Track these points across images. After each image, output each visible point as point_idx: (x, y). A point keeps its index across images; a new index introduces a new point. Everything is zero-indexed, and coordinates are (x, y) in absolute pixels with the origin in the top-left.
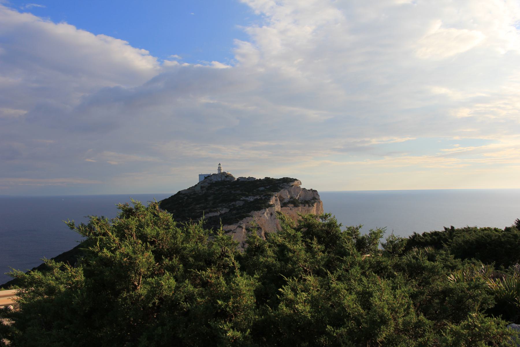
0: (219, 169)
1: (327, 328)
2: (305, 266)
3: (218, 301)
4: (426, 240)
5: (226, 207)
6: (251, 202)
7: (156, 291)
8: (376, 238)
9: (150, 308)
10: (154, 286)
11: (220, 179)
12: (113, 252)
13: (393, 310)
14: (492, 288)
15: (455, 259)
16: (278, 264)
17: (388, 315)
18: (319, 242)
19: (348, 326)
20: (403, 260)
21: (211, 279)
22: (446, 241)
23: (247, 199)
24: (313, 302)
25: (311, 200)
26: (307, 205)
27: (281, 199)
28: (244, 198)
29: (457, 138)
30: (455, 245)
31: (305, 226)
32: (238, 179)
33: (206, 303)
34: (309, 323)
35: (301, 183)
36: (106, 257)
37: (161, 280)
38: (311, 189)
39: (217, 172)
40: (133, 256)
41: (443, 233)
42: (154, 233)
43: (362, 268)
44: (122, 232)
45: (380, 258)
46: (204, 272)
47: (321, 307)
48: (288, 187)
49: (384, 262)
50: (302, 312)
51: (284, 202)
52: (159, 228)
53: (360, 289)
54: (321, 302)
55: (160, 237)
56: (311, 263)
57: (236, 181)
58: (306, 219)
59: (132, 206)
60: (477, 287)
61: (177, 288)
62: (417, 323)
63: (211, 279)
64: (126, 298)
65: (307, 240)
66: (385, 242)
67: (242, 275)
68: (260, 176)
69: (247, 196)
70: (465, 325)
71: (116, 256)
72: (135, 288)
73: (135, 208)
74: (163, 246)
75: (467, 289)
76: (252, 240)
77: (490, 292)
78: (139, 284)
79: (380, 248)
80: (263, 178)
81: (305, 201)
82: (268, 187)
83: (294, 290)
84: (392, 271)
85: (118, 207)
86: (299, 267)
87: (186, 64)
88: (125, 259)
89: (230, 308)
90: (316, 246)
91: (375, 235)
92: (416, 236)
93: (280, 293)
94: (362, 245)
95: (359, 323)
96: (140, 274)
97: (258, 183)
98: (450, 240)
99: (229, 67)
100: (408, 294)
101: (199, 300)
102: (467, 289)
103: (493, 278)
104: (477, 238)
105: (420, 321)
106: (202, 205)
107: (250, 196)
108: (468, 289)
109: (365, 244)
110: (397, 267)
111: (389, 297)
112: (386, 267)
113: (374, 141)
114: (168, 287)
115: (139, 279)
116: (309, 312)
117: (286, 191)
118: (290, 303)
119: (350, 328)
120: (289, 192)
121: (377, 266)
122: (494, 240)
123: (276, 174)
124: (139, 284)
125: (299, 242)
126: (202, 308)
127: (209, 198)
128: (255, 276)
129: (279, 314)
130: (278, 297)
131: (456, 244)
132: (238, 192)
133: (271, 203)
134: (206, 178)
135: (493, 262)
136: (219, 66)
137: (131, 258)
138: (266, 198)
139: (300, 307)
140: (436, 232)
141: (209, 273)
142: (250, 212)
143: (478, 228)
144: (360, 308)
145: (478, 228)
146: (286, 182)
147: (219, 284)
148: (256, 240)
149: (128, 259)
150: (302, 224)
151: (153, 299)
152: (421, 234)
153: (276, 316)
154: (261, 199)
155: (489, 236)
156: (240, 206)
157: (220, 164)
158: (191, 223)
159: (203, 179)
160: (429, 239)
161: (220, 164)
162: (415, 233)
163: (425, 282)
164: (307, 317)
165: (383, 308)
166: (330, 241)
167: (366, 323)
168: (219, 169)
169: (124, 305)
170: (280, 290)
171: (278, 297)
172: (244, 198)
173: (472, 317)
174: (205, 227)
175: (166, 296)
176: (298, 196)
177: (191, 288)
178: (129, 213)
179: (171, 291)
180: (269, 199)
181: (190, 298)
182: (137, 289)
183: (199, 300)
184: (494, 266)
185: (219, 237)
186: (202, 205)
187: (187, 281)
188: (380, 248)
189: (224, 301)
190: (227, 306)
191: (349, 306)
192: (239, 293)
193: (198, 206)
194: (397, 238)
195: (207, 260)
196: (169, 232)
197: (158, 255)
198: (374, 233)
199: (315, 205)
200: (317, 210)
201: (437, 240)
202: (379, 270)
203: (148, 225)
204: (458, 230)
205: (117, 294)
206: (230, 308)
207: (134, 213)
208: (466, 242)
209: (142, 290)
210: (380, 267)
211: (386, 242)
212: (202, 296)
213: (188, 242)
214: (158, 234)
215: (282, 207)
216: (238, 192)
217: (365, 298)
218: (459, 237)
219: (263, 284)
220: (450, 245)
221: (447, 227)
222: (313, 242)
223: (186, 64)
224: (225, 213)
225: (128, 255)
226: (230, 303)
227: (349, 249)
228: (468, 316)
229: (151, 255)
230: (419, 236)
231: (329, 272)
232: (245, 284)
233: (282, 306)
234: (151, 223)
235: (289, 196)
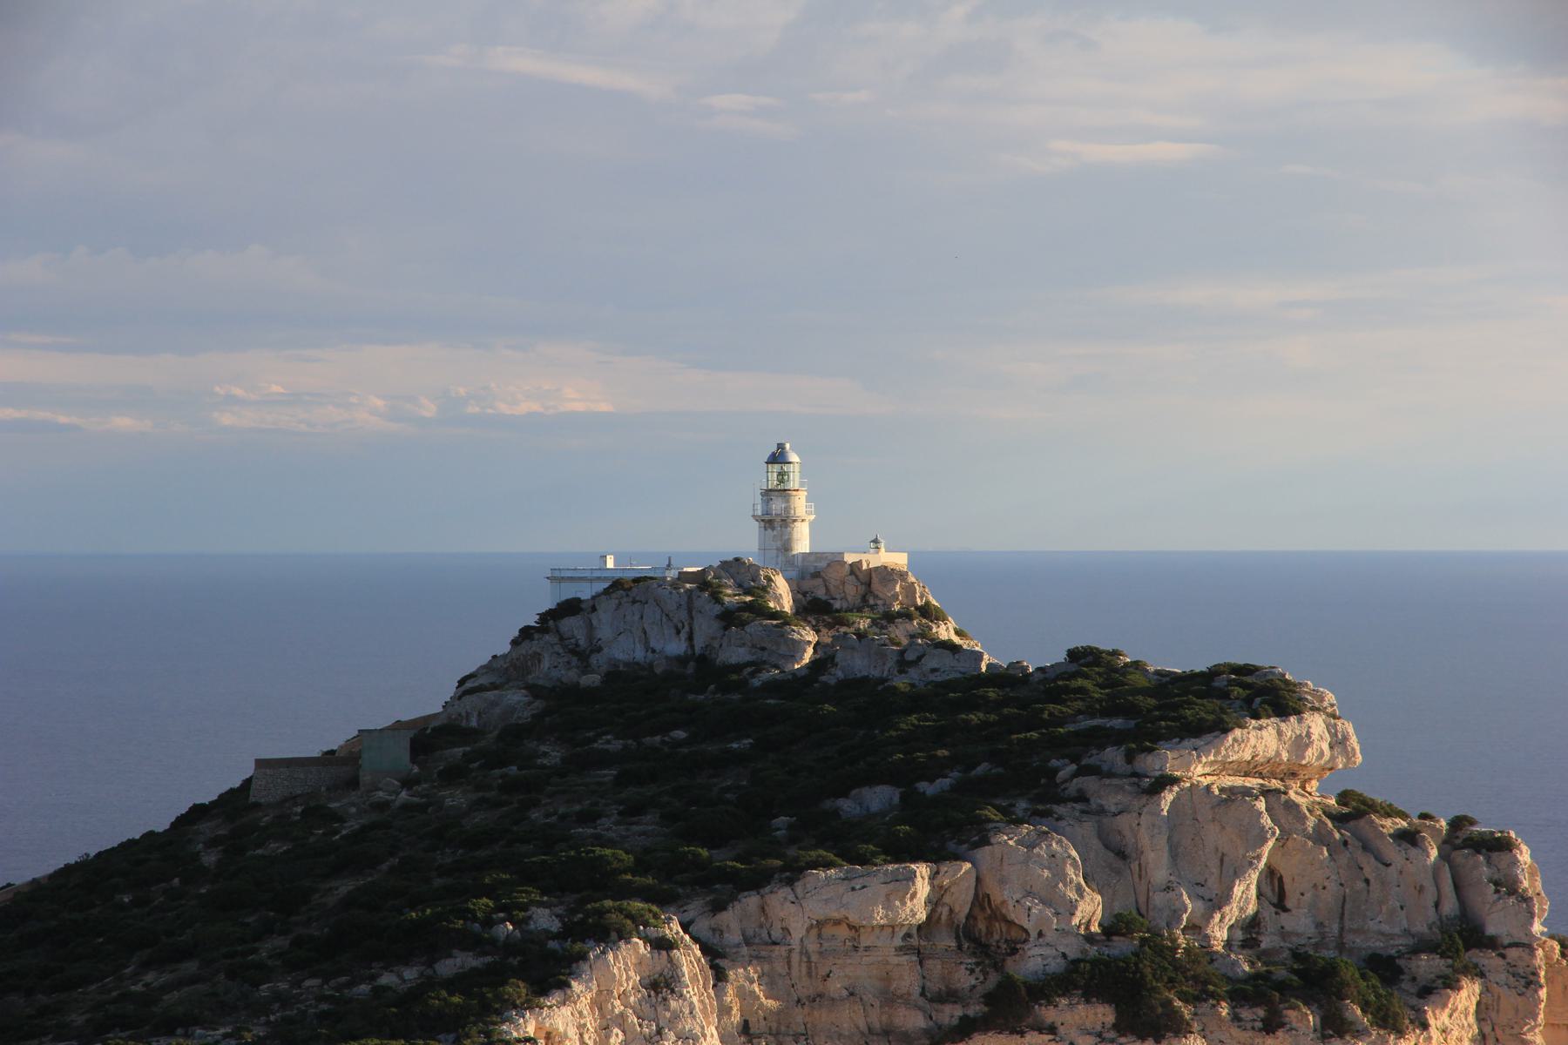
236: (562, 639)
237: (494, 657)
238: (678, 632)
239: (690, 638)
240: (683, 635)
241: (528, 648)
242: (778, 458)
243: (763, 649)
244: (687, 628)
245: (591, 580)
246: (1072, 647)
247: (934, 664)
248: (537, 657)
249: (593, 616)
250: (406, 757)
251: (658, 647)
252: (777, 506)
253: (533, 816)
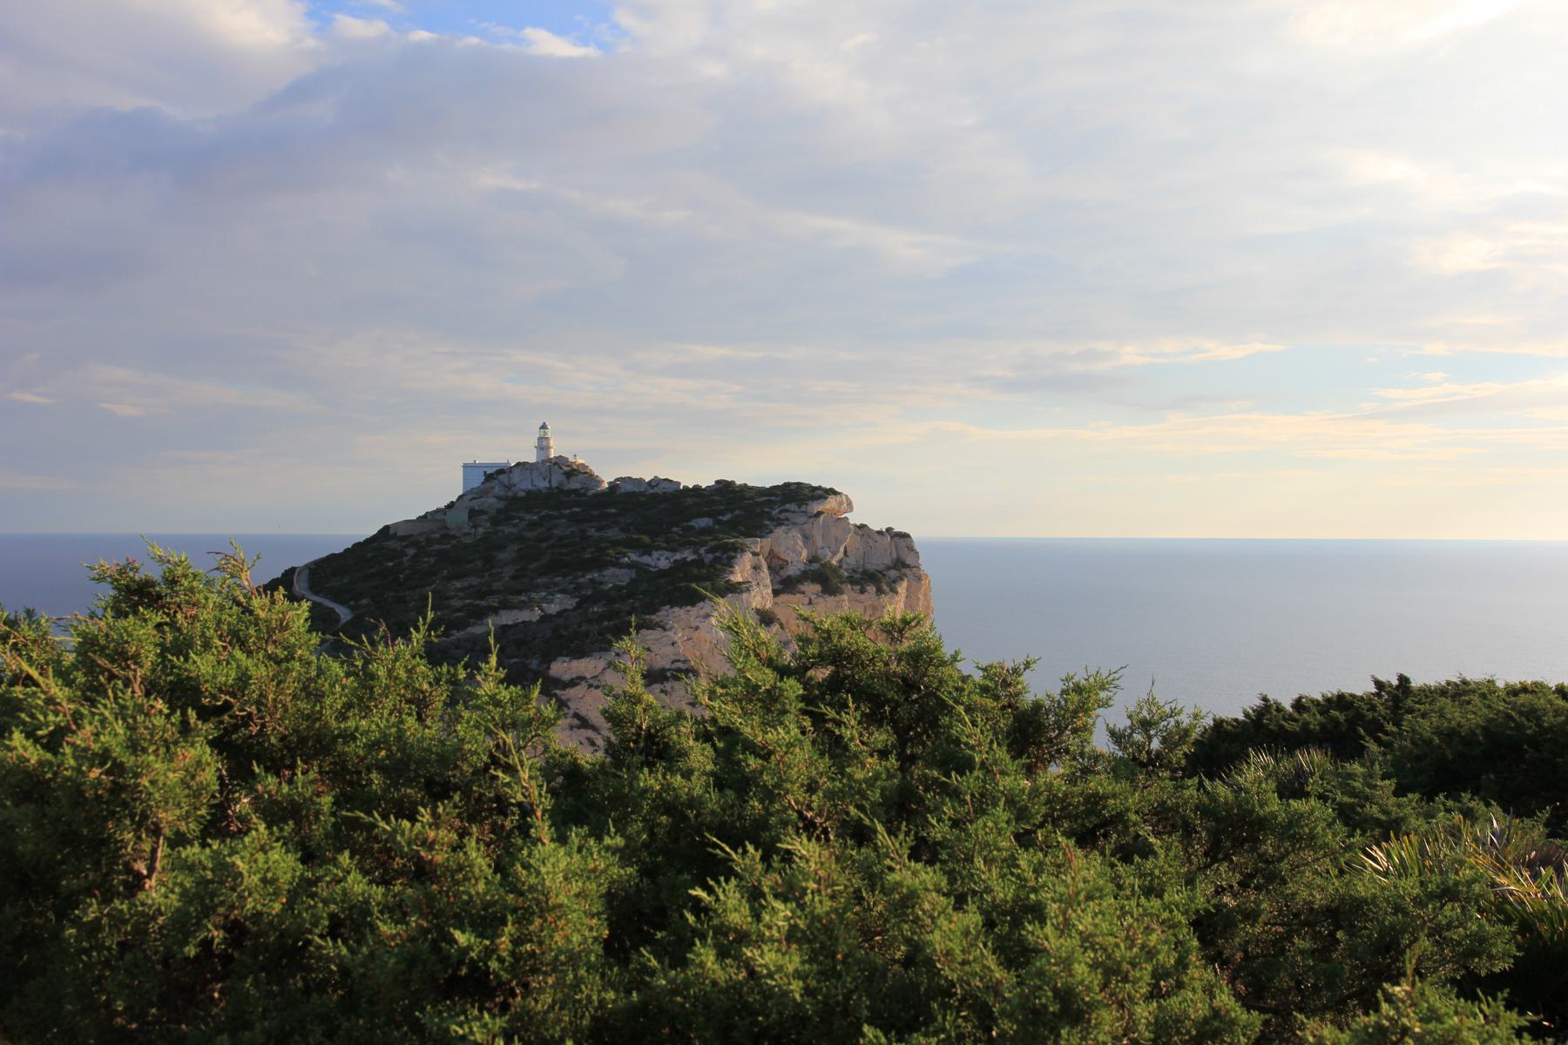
0: (543, 445)
1: (863, 1035)
2: (810, 808)
3: (457, 934)
4: (1306, 724)
5: (563, 591)
6: (662, 573)
7: (213, 895)
8: (1083, 708)
9: (187, 959)
10: (209, 875)
11: (543, 485)
12: (53, 743)
13: (1111, 971)
14: (1522, 903)
15: (1396, 794)
16: (713, 801)
17: (1089, 989)
18: (872, 720)
19: (943, 1030)
20: (1187, 793)
21: (431, 847)
22: (1375, 728)
23: (646, 559)
24: (814, 939)
25: (889, 568)
26: (871, 589)
27: (776, 565)
28: (634, 557)
29: (1436, 348)
30: (1407, 743)
31: (821, 660)
32: (613, 486)
33: (412, 940)
34: (801, 1020)
35: (850, 504)
36: (21, 766)
37: (233, 852)
38: (889, 530)
39: (532, 458)
40: (129, 760)
41: (1367, 701)
42: (228, 676)
43: (1021, 814)
44: (96, 667)
45: (1100, 783)
46: (406, 824)
47: (846, 956)
48: (801, 519)
49: (1114, 796)
50: (770, 976)
51: (784, 574)
52: (249, 653)
53: (1003, 892)
54: (846, 942)
55: (253, 691)
56: (830, 795)
57: (603, 494)
58: (828, 632)
59: (155, 573)
60: (1448, 894)
61: (304, 887)
62: (1206, 1021)
63: (431, 847)
64: (95, 926)
65: (824, 709)
66: (1122, 723)
67: (562, 839)
68: (695, 474)
70: (1366, 1027)
71: (62, 763)
72: (136, 883)
73: (166, 579)
74: (263, 726)
75: (1414, 900)
76: (623, 709)
77: (1502, 909)
78: (151, 869)
79: (1100, 742)
80: (707, 481)
81: (865, 572)
82: (727, 517)
83: (754, 895)
84: (1145, 830)
85: (94, 574)
86: (785, 810)
87: (423, 35)
88: (95, 773)
89: (501, 960)
90: (850, 727)
91: (1082, 699)
92: (1267, 708)
93: (698, 907)
94: (1030, 733)
95: (985, 1018)
96: (156, 831)
97: (690, 501)
98: (1390, 727)
99: (589, 51)
100: (1185, 913)
101: (386, 929)
102: (1414, 900)
103: (1530, 865)
104: (1490, 720)
105: (1215, 1013)
106: (475, 581)
107: (658, 548)
108: (1419, 902)
109: (1040, 728)
110: (1165, 817)
111: (1093, 916)
112: (1119, 818)
113: (1131, 354)
114: (264, 880)
115: (154, 851)
116: (798, 975)
117: (795, 534)
118: (731, 944)
119: (949, 1037)
120: (807, 538)
121: (1089, 813)
122: (1550, 729)
123: (758, 468)
124: (151, 869)
125: (789, 719)
126: (392, 961)
127: (502, 556)
128: (607, 841)
129: (687, 984)
130: (691, 919)
131: (1413, 743)
132: (613, 533)
133: (737, 577)
134: (489, 477)
135: (1541, 809)
136: (550, 45)
137: (118, 768)
138: (716, 560)
139: (765, 957)
140: (1341, 697)
141: (431, 831)
142: (655, 611)
143: (1500, 684)
144: (991, 961)
145: (1500, 684)
146: (795, 500)
147: (461, 868)
148: (639, 708)
149: (107, 773)
150: (813, 650)
151: (199, 925)
152: (1287, 705)
153: (675, 992)
154: (699, 563)
155: (1532, 713)
156: (620, 588)
157: (544, 427)
158: (384, 637)
159: (478, 480)
160: (1314, 720)
161: (544, 427)
162: (1265, 699)
163: (1266, 876)
164: (785, 994)
165: (1067, 963)
166: (908, 720)
167: (1010, 1016)
168: (543, 445)
169: (87, 952)
170: (698, 892)
171: (691, 919)
172: (634, 557)
173: (1389, 999)
174: (433, 655)
175: (258, 915)
176: (840, 555)
177: (357, 884)
178: (136, 595)
179: (276, 894)
180: (729, 564)
181: (351, 923)
182: (142, 888)
183: (386, 929)
184: (1546, 825)
185: (480, 692)
186: (475, 581)
187: (345, 858)
188: (1100, 742)
189: (481, 935)
190: (489, 952)
191: (949, 953)
192: (538, 902)
193: (458, 585)
194: (1167, 709)
195: (430, 778)
196: (288, 671)
197: (240, 755)
198: (1078, 689)
199: (902, 588)
200: (909, 605)
201: (1340, 726)
202: (1091, 826)
203: (207, 646)
204: (1428, 694)
205: (67, 905)
206: (501, 960)
207: (159, 597)
208: (1450, 735)
209: (160, 894)
210: (1099, 814)
211: (1128, 723)
212: (397, 911)
213: (366, 711)
214: (244, 679)
215: (776, 593)
216: (613, 533)
217: (1009, 930)
218: (1424, 716)
219: (644, 872)
220: (1388, 745)
221: (1383, 679)
222: (845, 718)
223: (423, 35)
224: (560, 614)
225: (104, 756)
226: (504, 942)
227: (972, 748)
228: (1379, 994)
229: (207, 758)
230: (1279, 709)
231: (880, 827)
232: (571, 877)
233: (706, 956)
234: (221, 637)
235: (805, 554)
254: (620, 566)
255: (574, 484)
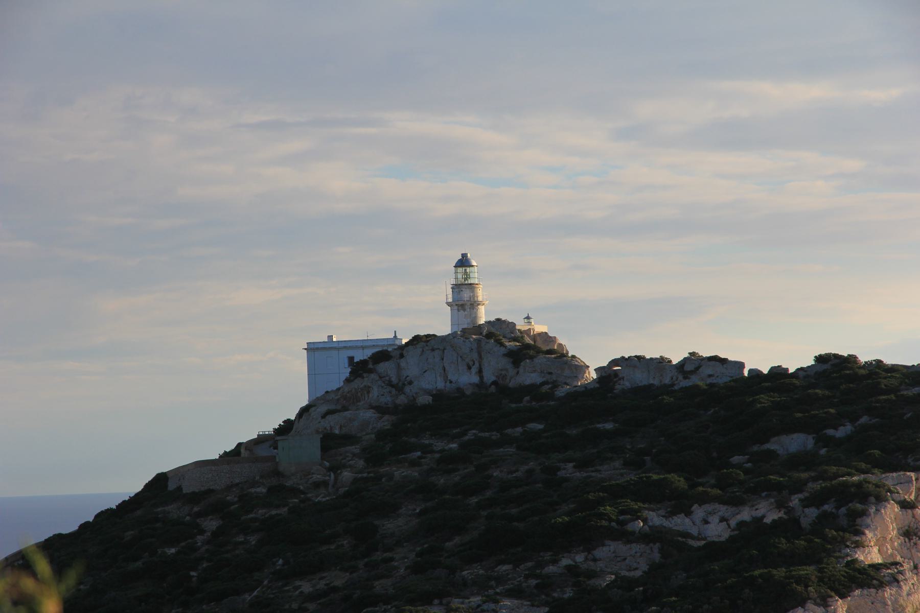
0: (463, 299)
11: (467, 379)
23: (680, 522)
28: (656, 518)
32: (607, 375)
69: (681, 504)
80: (797, 357)
157: (464, 262)
168: (463, 299)
172: (656, 518)
236: (381, 377)
237: (327, 392)
238: (469, 368)
239: (480, 371)
240: (474, 369)
241: (358, 383)
242: (464, 262)
243: (550, 373)
244: (477, 364)
245: (363, 348)
246: (823, 352)
247: (709, 371)
248: (368, 389)
249: (403, 363)
250: (318, 453)
251: (454, 379)
252: (466, 295)
253: (495, 474)
254: (629, 537)
255: (528, 376)
